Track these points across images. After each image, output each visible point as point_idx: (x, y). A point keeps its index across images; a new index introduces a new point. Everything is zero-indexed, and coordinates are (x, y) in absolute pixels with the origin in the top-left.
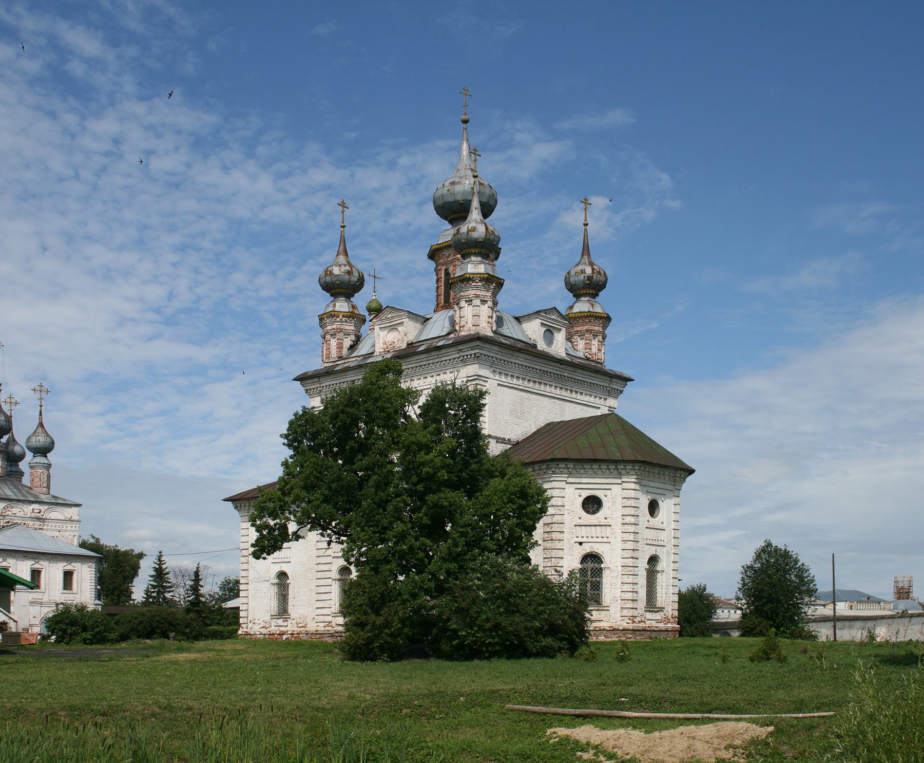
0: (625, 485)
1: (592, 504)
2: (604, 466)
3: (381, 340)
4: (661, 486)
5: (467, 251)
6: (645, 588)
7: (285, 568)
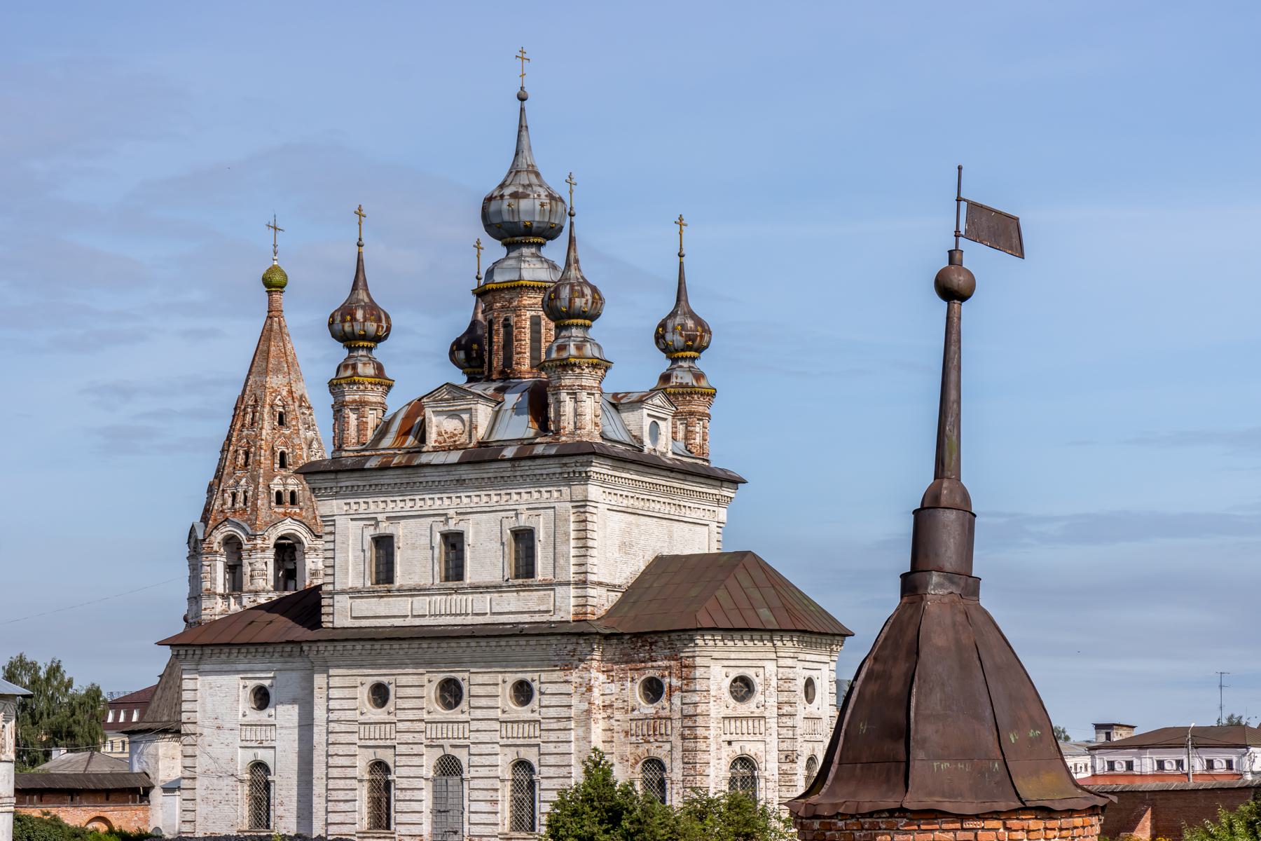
0: (781, 662)
1: (743, 688)
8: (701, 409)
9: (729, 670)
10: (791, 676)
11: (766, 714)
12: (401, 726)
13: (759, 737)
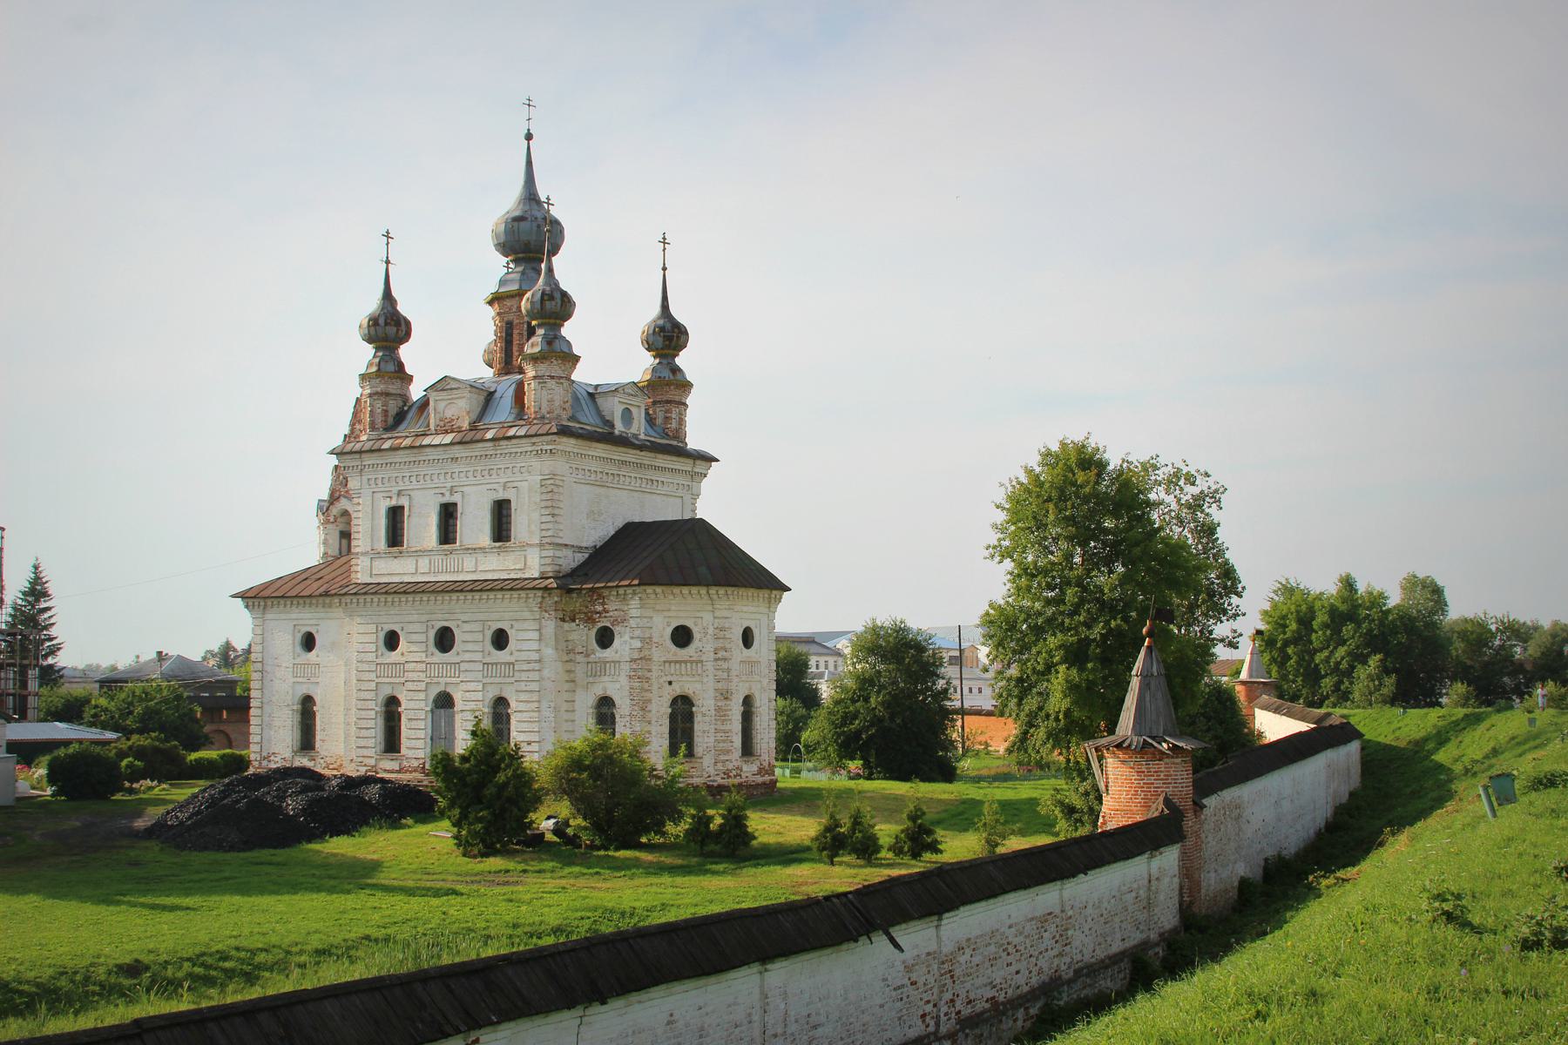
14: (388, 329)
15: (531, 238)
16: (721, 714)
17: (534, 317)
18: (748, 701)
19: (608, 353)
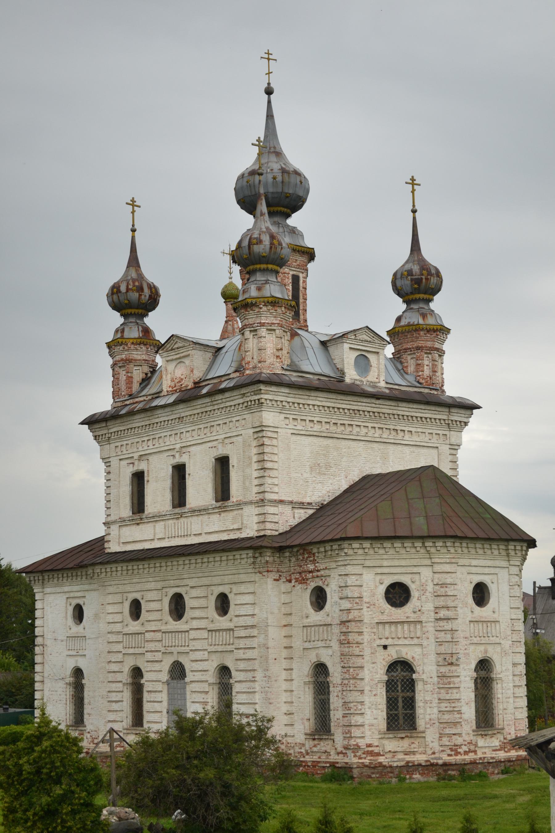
0: (437, 568)
1: (398, 594)
2: (408, 544)
3: (169, 377)
4: (489, 563)
5: (251, 267)
6: (473, 705)
7: (82, 664)
8: (429, 344)
9: (384, 577)
10: (449, 581)
11: (423, 619)
12: (148, 636)
13: (416, 641)
14: (134, 300)
15: (273, 194)
16: (446, 681)
17: (269, 267)
18: (484, 665)
19: (347, 296)
